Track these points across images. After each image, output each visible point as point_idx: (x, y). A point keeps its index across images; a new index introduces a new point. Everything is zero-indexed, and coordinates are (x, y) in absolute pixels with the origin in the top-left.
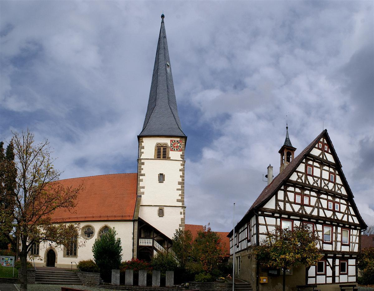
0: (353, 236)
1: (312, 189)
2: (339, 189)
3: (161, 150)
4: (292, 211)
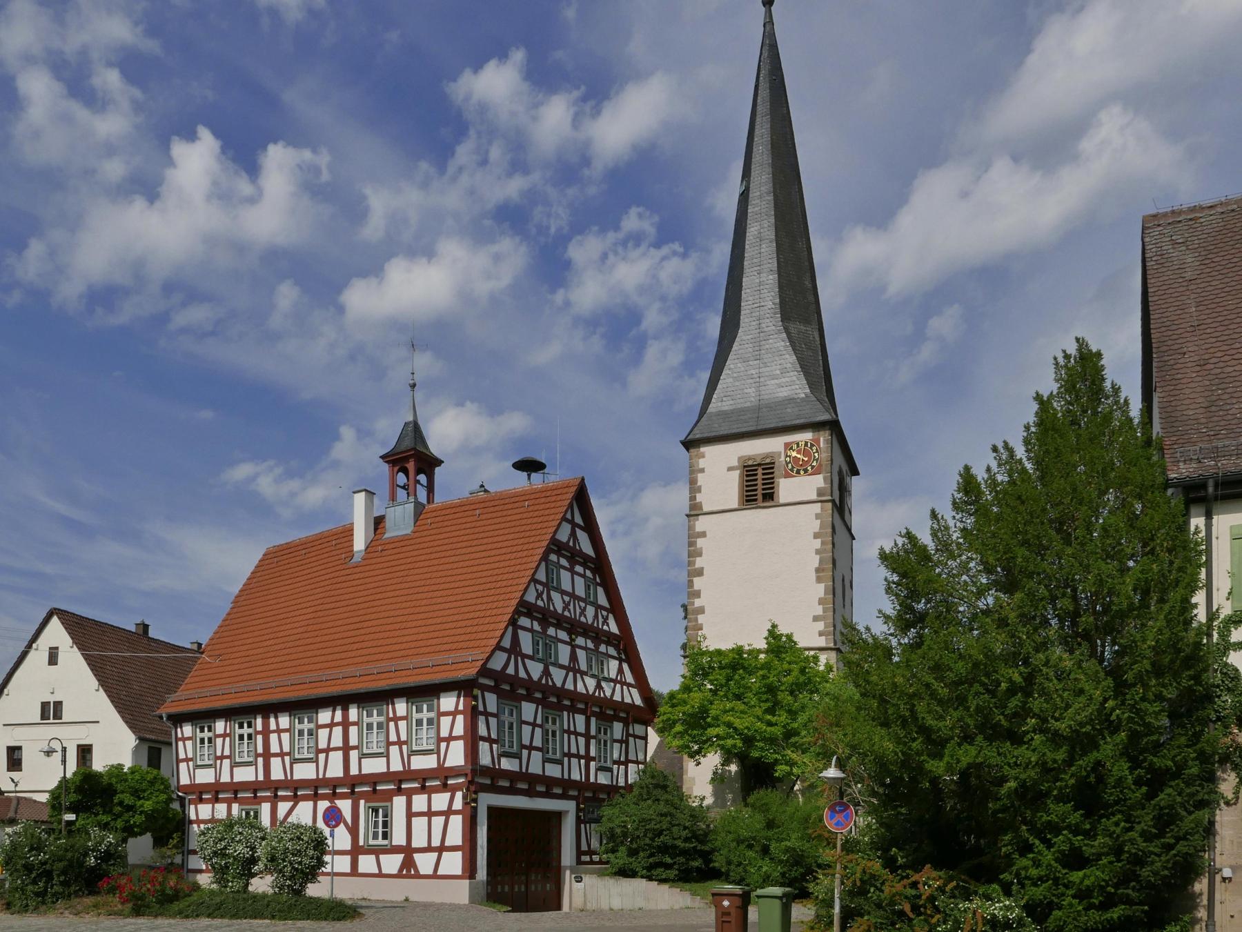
0: (186, 742)
1: (560, 621)
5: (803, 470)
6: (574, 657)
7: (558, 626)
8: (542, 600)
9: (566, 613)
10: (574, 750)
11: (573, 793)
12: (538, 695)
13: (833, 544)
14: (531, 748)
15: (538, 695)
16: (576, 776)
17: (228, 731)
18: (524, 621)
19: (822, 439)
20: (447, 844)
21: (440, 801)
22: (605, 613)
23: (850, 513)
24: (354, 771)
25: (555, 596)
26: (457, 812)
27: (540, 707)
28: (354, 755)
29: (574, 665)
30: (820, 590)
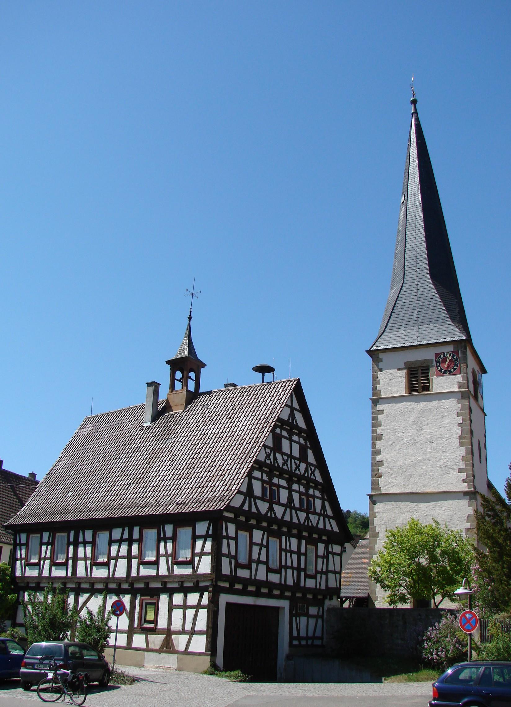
1: (282, 473)
2: (313, 473)
3: (422, 373)
4: (331, 529)
5: (449, 371)
6: (290, 498)
7: (280, 477)
8: (270, 459)
9: (285, 467)
10: (289, 564)
11: (287, 594)
12: (265, 524)
13: (471, 420)
14: (259, 562)
15: (265, 524)
16: (290, 582)
17: (50, 541)
18: (257, 474)
19: (460, 351)
20: (190, 650)
21: (193, 598)
22: (313, 468)
23: (482, 398)
24: (134, 573)
25: (278, 456)
26: (204, 607)
27: (266, 533)
28: (135, 562)
29: (291, 504)
30: (462, 451)
